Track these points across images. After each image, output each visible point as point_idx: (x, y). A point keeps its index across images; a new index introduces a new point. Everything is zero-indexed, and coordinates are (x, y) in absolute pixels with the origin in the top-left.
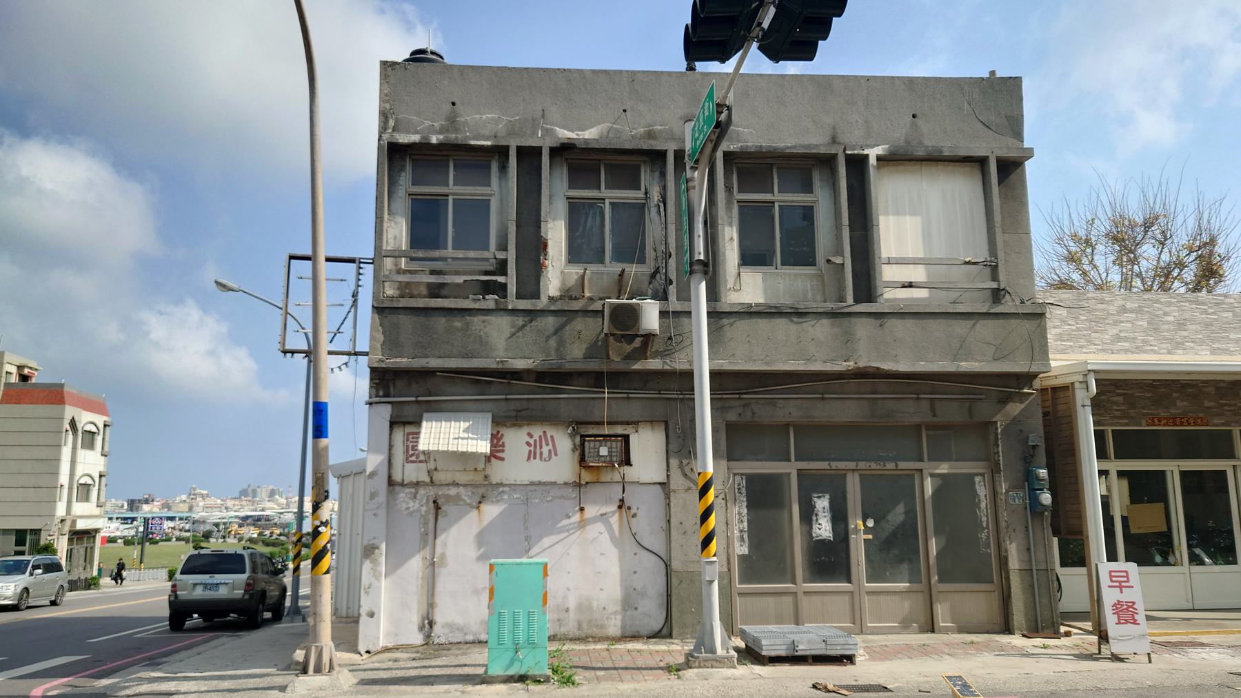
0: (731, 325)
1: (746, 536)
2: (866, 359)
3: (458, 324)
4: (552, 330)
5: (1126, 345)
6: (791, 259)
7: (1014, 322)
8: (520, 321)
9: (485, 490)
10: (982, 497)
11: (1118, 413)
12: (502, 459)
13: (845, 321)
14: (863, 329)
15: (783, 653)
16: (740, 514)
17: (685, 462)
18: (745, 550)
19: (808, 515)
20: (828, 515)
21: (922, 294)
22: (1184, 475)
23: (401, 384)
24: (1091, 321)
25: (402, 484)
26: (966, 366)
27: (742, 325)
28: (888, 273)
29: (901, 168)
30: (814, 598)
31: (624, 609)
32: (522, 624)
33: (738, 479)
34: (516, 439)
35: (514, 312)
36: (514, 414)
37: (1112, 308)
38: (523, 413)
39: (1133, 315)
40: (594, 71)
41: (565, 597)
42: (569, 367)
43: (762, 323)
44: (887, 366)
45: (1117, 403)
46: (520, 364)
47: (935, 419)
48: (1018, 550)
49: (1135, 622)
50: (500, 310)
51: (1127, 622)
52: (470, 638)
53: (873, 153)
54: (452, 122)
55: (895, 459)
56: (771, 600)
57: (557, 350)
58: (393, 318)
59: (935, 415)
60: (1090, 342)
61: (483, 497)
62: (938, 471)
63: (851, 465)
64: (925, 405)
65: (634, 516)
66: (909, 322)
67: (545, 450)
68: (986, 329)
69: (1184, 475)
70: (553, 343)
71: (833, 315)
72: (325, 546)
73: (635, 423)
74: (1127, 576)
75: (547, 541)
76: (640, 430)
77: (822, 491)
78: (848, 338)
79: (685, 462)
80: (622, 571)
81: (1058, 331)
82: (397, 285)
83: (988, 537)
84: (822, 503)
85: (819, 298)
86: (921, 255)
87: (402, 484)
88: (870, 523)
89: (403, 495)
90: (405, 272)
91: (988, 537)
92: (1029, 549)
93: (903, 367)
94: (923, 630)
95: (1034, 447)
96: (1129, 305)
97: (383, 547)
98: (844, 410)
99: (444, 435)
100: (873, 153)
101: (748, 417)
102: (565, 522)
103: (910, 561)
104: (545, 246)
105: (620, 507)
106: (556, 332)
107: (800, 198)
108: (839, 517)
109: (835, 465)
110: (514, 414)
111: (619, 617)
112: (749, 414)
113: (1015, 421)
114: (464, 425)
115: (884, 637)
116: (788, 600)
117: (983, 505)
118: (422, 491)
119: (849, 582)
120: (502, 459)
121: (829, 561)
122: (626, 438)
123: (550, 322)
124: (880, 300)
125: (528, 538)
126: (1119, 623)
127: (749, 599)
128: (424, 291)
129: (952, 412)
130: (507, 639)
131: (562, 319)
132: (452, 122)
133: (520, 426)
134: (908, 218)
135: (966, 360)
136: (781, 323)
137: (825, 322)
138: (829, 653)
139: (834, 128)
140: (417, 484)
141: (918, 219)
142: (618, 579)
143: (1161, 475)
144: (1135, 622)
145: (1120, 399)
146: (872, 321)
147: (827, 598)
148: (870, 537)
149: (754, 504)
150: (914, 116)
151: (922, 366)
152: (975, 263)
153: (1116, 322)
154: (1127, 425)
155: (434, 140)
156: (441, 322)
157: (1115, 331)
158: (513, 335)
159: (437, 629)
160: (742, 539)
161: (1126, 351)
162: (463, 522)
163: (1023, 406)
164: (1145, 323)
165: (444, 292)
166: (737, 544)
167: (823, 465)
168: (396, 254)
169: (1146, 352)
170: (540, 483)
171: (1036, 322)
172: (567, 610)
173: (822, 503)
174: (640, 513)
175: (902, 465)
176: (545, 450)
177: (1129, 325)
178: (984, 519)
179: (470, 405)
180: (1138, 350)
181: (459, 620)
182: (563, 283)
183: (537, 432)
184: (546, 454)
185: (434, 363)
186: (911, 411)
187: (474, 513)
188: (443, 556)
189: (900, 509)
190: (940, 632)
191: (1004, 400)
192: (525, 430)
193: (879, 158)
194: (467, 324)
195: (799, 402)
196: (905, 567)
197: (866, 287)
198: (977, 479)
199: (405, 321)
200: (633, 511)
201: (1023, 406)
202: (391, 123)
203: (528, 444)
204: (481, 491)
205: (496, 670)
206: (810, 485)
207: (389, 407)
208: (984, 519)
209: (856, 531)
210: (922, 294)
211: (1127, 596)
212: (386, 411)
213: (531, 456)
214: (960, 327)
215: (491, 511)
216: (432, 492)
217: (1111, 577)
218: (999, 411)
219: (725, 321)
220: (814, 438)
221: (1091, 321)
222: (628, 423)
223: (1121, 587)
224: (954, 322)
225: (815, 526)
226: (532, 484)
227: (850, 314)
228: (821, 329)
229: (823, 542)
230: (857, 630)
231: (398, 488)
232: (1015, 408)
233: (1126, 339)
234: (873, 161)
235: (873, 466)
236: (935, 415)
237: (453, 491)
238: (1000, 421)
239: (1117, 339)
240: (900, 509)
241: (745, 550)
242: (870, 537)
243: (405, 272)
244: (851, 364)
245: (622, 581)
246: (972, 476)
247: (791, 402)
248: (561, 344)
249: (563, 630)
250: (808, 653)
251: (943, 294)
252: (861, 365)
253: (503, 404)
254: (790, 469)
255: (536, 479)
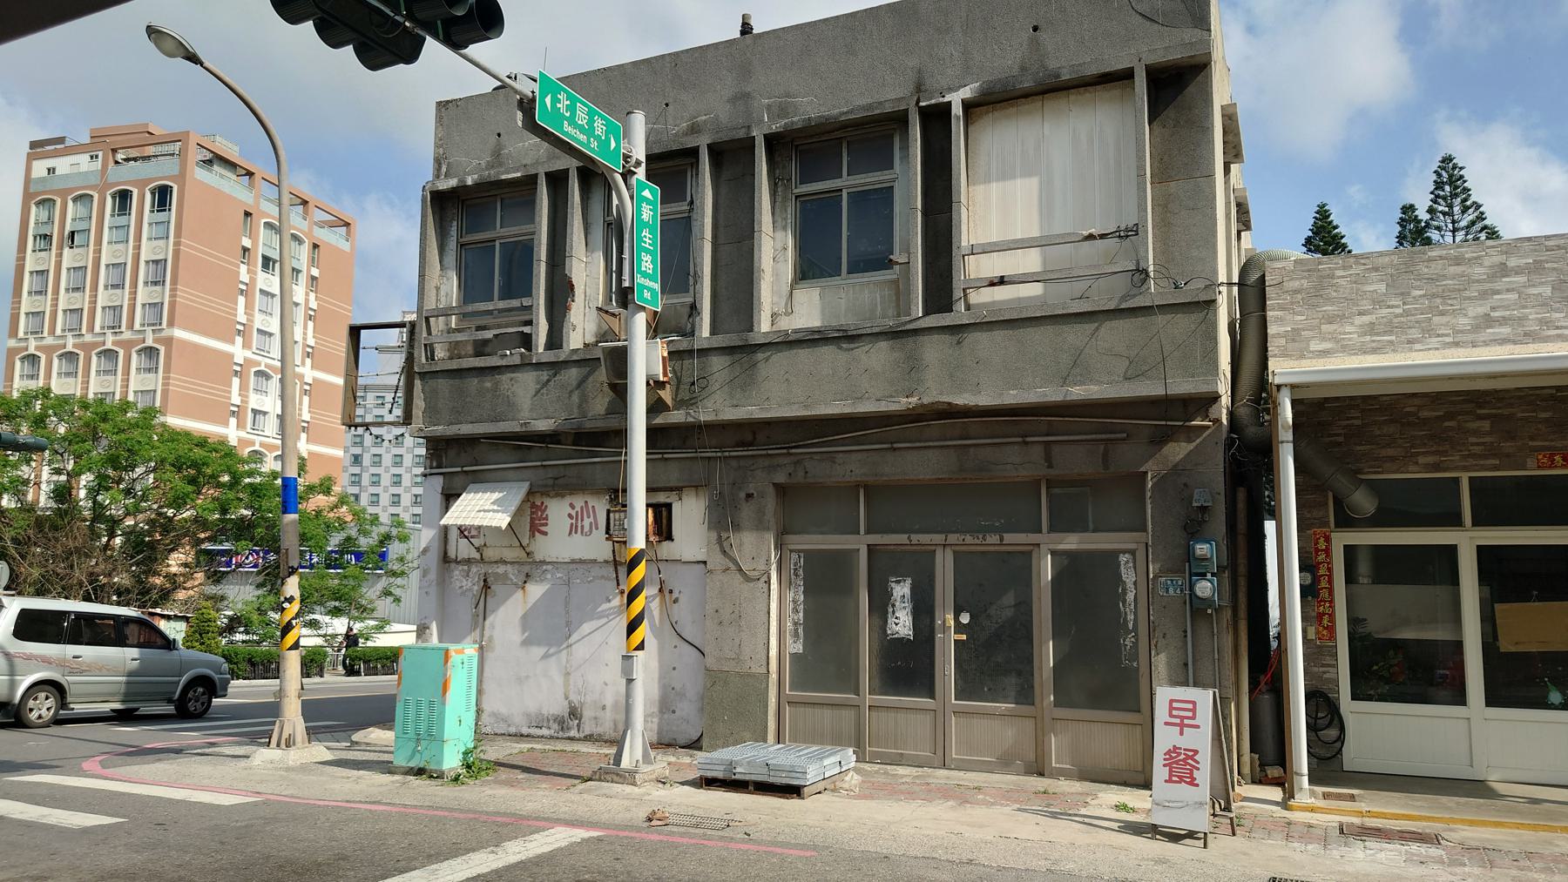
0: (767, 359)
1: (801, 631)
2: (935, 391)
3: (488, 385)
4: (575, 383)
5: (1505, 331)
6: (863, 264)
7: (1160, 319)
8: (545, 375)
9: (530, 568)
10: (1130, 585)
11: (1476, 449)
12: (545, 534)
13: (909, 342)
14: (933, 350)
15: (720, 775)
16: (794, 601)
17: (724, 535)
18: (798, 648)
19: (881, 605)
20: (908, 605)
21: (1035, 290)
22: (1482, 551)
23: (452, 453)
24: (1434, 296)
25: (457, 562)
26: (1078, 392)
27: (780, 359)
28: (976, 268)
29: (1013, 110)
30: (883, 715)
31: (661, 712)
32: (424, 713)
33: (794, 556)
34: (558, 511)
35: (539, 366)
36: (550, 482)
37: (1478, 270)
38: (560, 481)
39: (1521, 279)
40: (635, 63)
41: (602, 693)
42: (589, 425)
43: (803, 354)
44: (962, 399)
45: (1476, 432)
46: (543, 425)
47: (1052, 472)
48: (1168, 664)
49: (1193, 783)
50: (525, 365)
51: (1181, 780)
52: (513, 730)
53: (956, 99)
54: (497, 156)
55: (1000, 531)
56: (827, 712)
57: (580, 406)
58: (432, 383)
59: (1050, 466)
60: (1429, 331)
61: (527, 575)
62: (1061, 547)
63: (938, 538)
64: (1037, 453)
65: (676, 601)
66: (999, 335)
67: (587, 522)
68: (1114, 334)
69: (1482, 551)
70: (575, 398)
71: (894, 335)
72: (289, 623)
73: (678, 490)
74: (1194, 710)
75: (587, 627)
76: (684, 497)
77: (901, 575)
78: (913, 366)
79: (724, 535)
80: (661, 667)
81: (1366, 319)
82: (446, 346)
83: (1135, 644)
84: (901, 590)
85: (890, 312)
86: (1035, 233)
87: (457, 562)
88: (965, 619)
89: (457, 572)
90: (458, 330)
91: (1135, 644)
92: (1186, 665)
93: (984, 400)
94: (1029, 772)
95: (1203, 509)
96: (1513, 262)
97: (434, 627)
98: (921, 464)
99: (483, 509)
100: (956, 99)
101: (799, 477)
102: (605, 606)
103: (1019, 673)
104: (572, 287)
105: (661, 590)
106: (579, 385)
107: (871, 179)
108: (923, 609)
109: (915, 538)
110: (550, 482)
111: (656, 720)
112: (801, 474)
113: (1177, 470)
114: (496, 495)
115: (961, 774)
116: (848, 715)
117: (1130, 596)
118: (474, 569)
119: (933, 697)
120: (545, 534)
121: (907, 668)
122: (669, 506)
123: (573, 374)
124: (960, 306)
125: (568, 624)
126: (1169, 781)
127: (801, 709)
128: (470, 349)
129: (1077, 460)
130: (411, 730)
131: (585, 370)
132: (497, 156)
133: (563, 496)
134: (1019, 181)
135: (1082, 383)
136: (827, 351)
137: (883, 345)
138: (771, 780)
139: (919, 71)
140: (468, 561)
141: (1034, 182)
142: (656, 676)
143: (1451, 551)
144: (1193, 783)
145: (1486, 425)
146: (946, 338)
147: (901, 716)
148: (964, 637)
149: (814, 588)
150: (1035, 29)
151: (1012, 397)
152: (1103, 236)
153: (1484, 295)
154: (1496, 468)
155: (469, 182)
156: (473, 383)
157: (1481, 310)
158: (537, 393)
159: (485, 718)
160: (796, 634)
161: (1503, 341)
162: (512, 600)
163: (1192, 446)
164: (1547, 291)
165: (488, 350)
166: (789, 640)
167: (901, 538)
168: (446, 312)
169: (1546, 339)
170: (581, 562)
171: (1196, 317)
172: (604, 708)
173: (901, 590)
174: (683, 599)
175: (1009, 538)
176: (587, 522)
177: (1513, 296)
178: (1131, 617)
179: (511, 474)
180: (1530, 337)
181: (504, 711)
182: (599, 327)
183: (579, 502)
184: (587, 529)
185: (466, 429)
186: (1016, 462)
187: (520, 593)
188: (491, 639)
189: (1009, 599)
190: (1051, 776)
191: (1161, 438)
192: (568, 499)
193: (968, 106)
194: (496, 384)
195: (859, 456)
196: (1011, 681)
197: (940, 292)
198: (1123, 558)
199: (443, 384)
200: (675, 595)
201: (1192, 446)
202: (444, 169)
203: (570, 516)
204: (526, 569)
205: (400, 760)
206: (883, 566)
207: (441, 478)
208: (1131, 617)
209: (945, 628)
210: (1035, 290)
211: (1189, 740)
212: (438, 482)
213: (573, 529)
214: (1074, 335)
215: (536, 591)
216: (483, 569)
217: (1171, 708)
218: (1151, 457)
219: (760, 356)
220: (886, 500)
221: (1434, 296)
222: (671, 489)
223: (1182, 726)
224: (1066, 328)
225: (891, 620)
226: (573, 562)
227: (916, 332)
228: (878, 356)
229: (901, 641)
230: (938, 760)
231: (453, 565)
232: (1177, 451)
233: (1503, 321)
234: (957, 110)
235: (969, 539)
236: (1050, 466)
237: (501, 569)
238: (1152, 470)
239: (1488, 321)
240: (1009, 599)
241: (798, 648)
242: (964, 637)
243: (458, 330)
244: (914, 400)
245: (661, 678)
246: (1114, 554)
247: (854, 456)
248: (584, 399)
249: (600, 730)
250: (747, 778)
251: (1064, 288)
252: (926, 401)
253: (541, 471)
254: (859, 544)
255: (577, 557)
